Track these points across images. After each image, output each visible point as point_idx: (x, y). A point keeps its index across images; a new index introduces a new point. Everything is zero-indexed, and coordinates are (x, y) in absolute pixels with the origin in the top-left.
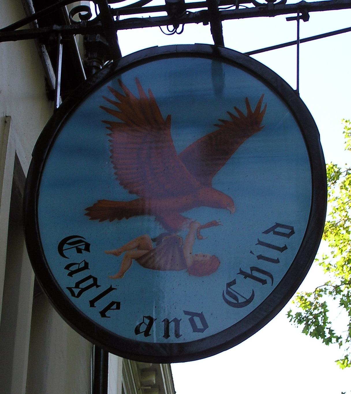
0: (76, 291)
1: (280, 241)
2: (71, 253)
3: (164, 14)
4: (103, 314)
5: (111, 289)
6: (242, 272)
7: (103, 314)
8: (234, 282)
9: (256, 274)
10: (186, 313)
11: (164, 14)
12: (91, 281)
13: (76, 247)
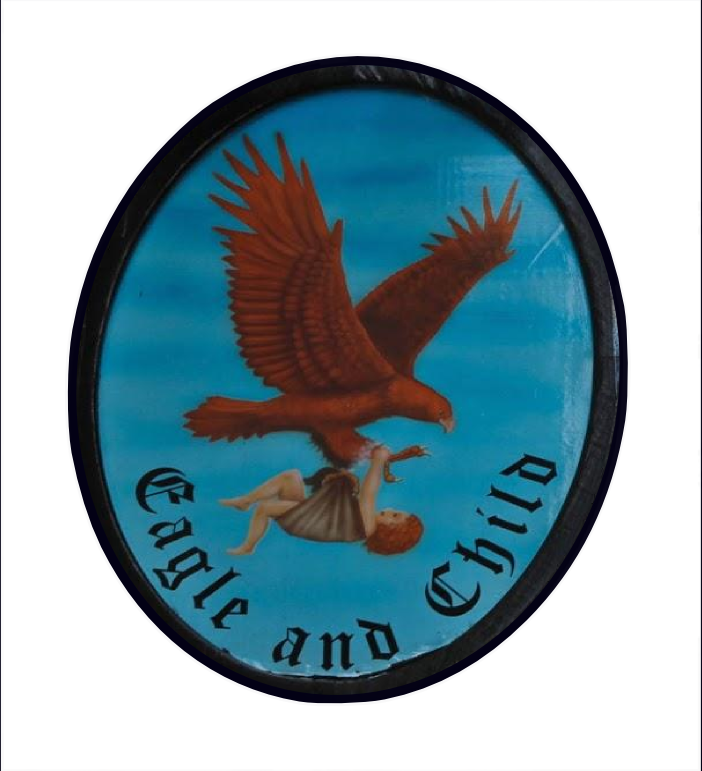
0: (171, 577)
1: (528, 490)
2: (158, 500)
5: (230, 575)
6: (460, 550)
7: (217, 621)
8: (445, 568)
9: (485, 553)
10: (363, 624)
12: (195, 559)
13: (169, 491)
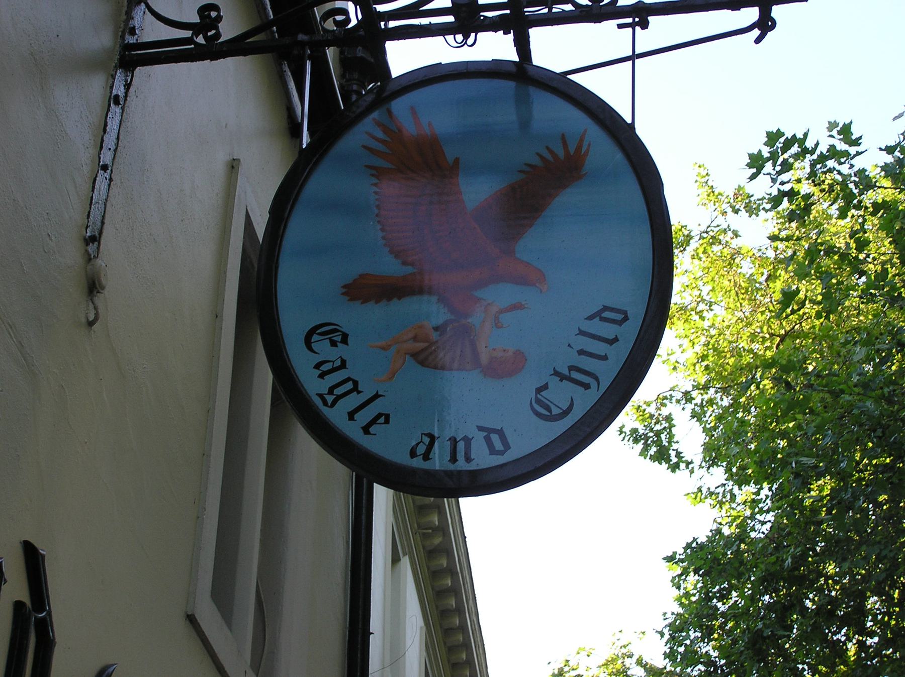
0: (330, 399)
2: (322, 346)
3: (450, 19)
4: (366, 430)
5: (377, 396)
6: (556, 373)
7: (366, 430)
8: (545, 387)
9: (575, 375)
10: (480, 429)
11: (450, 19)
12: (349, 386)
13: (330, 339)
